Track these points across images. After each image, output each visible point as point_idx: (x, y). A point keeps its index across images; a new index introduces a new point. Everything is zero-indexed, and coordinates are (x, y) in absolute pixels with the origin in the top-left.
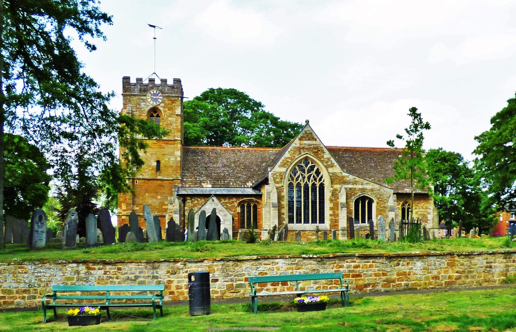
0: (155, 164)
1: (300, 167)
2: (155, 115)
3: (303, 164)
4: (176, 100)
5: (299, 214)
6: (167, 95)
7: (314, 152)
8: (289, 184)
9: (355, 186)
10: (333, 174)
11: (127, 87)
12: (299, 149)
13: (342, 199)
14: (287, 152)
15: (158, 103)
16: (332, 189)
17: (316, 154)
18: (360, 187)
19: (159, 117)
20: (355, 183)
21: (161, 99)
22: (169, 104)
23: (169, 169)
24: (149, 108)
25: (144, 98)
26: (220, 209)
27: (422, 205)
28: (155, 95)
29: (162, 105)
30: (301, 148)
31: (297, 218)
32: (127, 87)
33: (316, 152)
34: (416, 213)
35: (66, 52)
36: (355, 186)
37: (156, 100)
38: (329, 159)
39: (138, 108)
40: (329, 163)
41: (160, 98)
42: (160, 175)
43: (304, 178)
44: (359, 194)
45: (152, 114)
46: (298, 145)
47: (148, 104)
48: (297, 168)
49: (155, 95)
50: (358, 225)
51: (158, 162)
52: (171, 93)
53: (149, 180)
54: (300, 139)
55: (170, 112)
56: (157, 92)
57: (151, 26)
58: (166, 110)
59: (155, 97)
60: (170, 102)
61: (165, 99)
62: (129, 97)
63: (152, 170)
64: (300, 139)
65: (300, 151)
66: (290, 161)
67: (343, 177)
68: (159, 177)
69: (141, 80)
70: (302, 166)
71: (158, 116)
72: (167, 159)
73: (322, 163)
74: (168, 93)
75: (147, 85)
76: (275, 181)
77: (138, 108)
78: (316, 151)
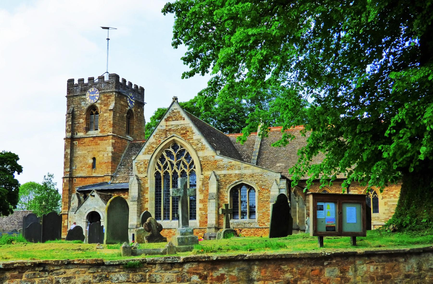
0: (91, 161)
1: (169, 154)
2: (94, 113)
3: (171, 150)
4: (111, 96)
5: (166, 210)
6: (103, 91)
7: (182, 134)
8: (156, 173)
9: (230, 172)
10: (203, 158)
11: (71, 88)
12: (166, 132)
13: (213, 189)
14: (152, 136)
15: (95, 101)
16: (202, 177)
17: (184, 135)
18: (237, 172)
19: (98, 114)
20: (231, 167)
21: (97, 96)
22: (104, 101)
23: (103, 166)
24: (88, 105)
25: (84, 97)
26: (101, 205)
27: (393, 193)
28: (93, 93)
29: (99, 101)
30: (167, 131)
31: (173, 214)
32: (71, 88)
33: (184, 134)
34: (386, 204)
35: (425, 94)
36: (230, 172)
37: (93, 98)
38: (199, 141)
39: (79, 108)
40: (200, 145)
41: (97, 95)
42: (95, 172)
43: (172, 165)
44: (235, 181)
45: (92, 112)
46: (164, 128)
47: (87, 103)
48: (164, 154)
49: (93, 93)
50: (236, 221)
51: (94, 159)
52: (107, 89)
53: (85, 178)
54: (167, 120)
55: (105, 108)
56: (94, 89)
57: (104, 28)
58: (103, 106)
59: (92, 95)
60: (106, 98)
61: (102, 96)
62: (72, 98)
63: (88, 167)
64: (167, 120)
65: (166, 134)
66: (155, 146)
67: (216, 161)
68: (94, 175)
69: (83, 80)
70: (170, 152)
71: (97, 113)
72: (102, 156)
73: (191, 145)
74: (104, 90)
75: (87, 85)
76: (139, 171)
77: (79, 108)
78: (184, 132)
